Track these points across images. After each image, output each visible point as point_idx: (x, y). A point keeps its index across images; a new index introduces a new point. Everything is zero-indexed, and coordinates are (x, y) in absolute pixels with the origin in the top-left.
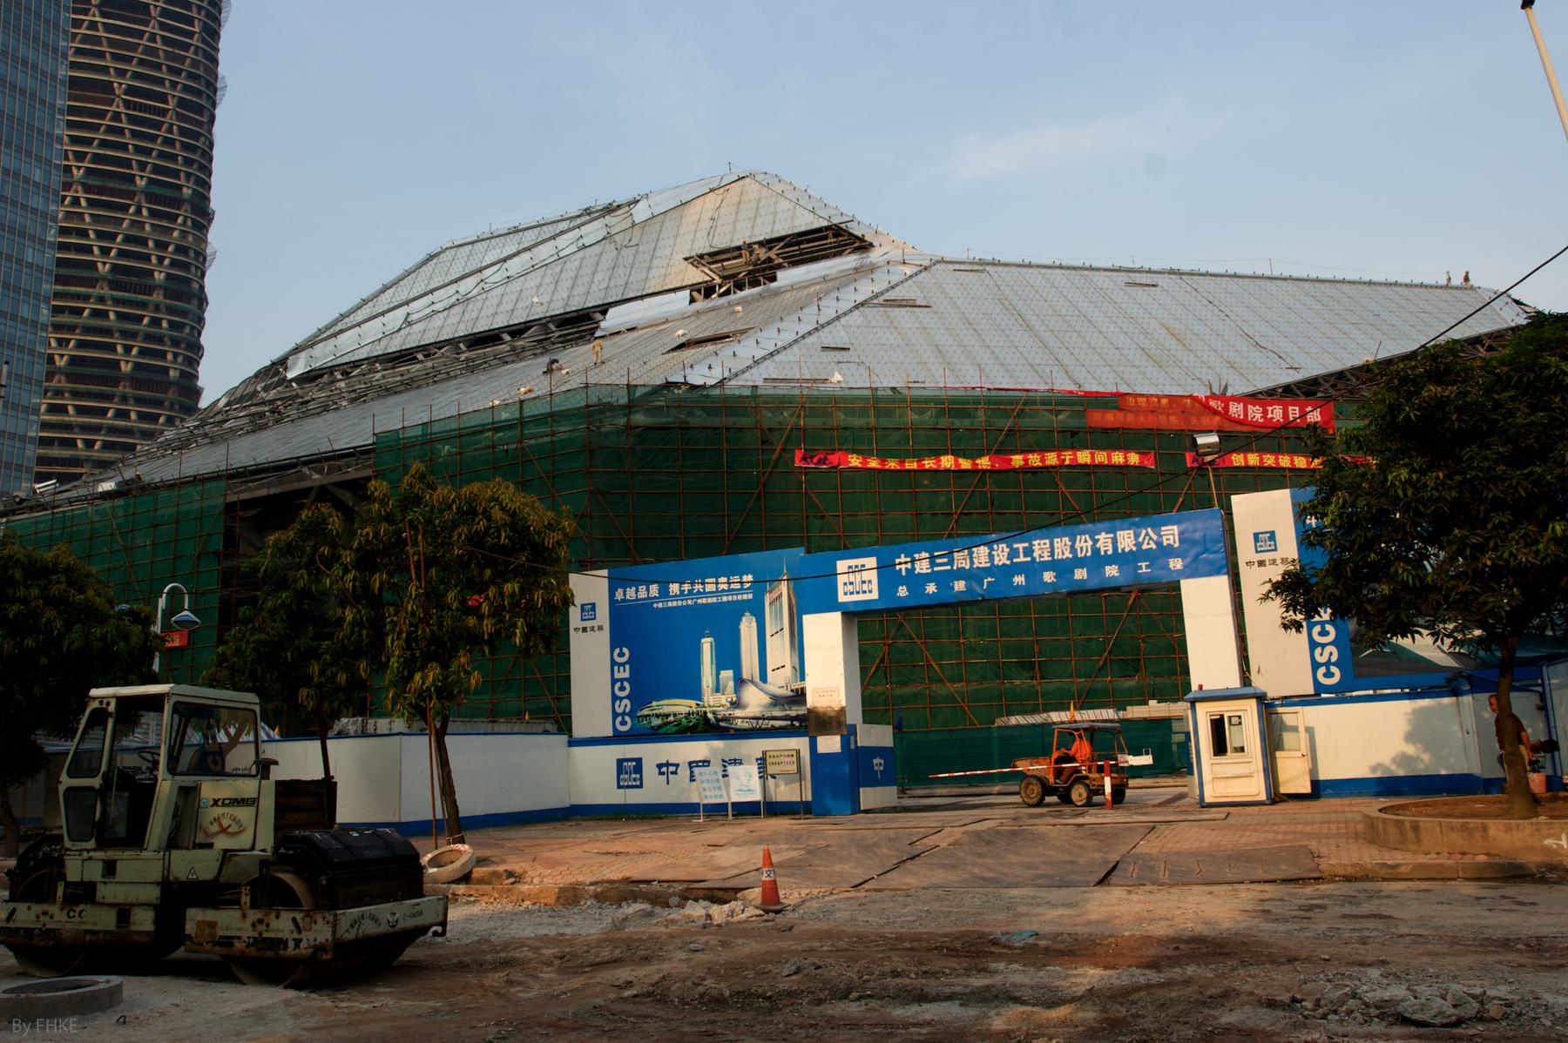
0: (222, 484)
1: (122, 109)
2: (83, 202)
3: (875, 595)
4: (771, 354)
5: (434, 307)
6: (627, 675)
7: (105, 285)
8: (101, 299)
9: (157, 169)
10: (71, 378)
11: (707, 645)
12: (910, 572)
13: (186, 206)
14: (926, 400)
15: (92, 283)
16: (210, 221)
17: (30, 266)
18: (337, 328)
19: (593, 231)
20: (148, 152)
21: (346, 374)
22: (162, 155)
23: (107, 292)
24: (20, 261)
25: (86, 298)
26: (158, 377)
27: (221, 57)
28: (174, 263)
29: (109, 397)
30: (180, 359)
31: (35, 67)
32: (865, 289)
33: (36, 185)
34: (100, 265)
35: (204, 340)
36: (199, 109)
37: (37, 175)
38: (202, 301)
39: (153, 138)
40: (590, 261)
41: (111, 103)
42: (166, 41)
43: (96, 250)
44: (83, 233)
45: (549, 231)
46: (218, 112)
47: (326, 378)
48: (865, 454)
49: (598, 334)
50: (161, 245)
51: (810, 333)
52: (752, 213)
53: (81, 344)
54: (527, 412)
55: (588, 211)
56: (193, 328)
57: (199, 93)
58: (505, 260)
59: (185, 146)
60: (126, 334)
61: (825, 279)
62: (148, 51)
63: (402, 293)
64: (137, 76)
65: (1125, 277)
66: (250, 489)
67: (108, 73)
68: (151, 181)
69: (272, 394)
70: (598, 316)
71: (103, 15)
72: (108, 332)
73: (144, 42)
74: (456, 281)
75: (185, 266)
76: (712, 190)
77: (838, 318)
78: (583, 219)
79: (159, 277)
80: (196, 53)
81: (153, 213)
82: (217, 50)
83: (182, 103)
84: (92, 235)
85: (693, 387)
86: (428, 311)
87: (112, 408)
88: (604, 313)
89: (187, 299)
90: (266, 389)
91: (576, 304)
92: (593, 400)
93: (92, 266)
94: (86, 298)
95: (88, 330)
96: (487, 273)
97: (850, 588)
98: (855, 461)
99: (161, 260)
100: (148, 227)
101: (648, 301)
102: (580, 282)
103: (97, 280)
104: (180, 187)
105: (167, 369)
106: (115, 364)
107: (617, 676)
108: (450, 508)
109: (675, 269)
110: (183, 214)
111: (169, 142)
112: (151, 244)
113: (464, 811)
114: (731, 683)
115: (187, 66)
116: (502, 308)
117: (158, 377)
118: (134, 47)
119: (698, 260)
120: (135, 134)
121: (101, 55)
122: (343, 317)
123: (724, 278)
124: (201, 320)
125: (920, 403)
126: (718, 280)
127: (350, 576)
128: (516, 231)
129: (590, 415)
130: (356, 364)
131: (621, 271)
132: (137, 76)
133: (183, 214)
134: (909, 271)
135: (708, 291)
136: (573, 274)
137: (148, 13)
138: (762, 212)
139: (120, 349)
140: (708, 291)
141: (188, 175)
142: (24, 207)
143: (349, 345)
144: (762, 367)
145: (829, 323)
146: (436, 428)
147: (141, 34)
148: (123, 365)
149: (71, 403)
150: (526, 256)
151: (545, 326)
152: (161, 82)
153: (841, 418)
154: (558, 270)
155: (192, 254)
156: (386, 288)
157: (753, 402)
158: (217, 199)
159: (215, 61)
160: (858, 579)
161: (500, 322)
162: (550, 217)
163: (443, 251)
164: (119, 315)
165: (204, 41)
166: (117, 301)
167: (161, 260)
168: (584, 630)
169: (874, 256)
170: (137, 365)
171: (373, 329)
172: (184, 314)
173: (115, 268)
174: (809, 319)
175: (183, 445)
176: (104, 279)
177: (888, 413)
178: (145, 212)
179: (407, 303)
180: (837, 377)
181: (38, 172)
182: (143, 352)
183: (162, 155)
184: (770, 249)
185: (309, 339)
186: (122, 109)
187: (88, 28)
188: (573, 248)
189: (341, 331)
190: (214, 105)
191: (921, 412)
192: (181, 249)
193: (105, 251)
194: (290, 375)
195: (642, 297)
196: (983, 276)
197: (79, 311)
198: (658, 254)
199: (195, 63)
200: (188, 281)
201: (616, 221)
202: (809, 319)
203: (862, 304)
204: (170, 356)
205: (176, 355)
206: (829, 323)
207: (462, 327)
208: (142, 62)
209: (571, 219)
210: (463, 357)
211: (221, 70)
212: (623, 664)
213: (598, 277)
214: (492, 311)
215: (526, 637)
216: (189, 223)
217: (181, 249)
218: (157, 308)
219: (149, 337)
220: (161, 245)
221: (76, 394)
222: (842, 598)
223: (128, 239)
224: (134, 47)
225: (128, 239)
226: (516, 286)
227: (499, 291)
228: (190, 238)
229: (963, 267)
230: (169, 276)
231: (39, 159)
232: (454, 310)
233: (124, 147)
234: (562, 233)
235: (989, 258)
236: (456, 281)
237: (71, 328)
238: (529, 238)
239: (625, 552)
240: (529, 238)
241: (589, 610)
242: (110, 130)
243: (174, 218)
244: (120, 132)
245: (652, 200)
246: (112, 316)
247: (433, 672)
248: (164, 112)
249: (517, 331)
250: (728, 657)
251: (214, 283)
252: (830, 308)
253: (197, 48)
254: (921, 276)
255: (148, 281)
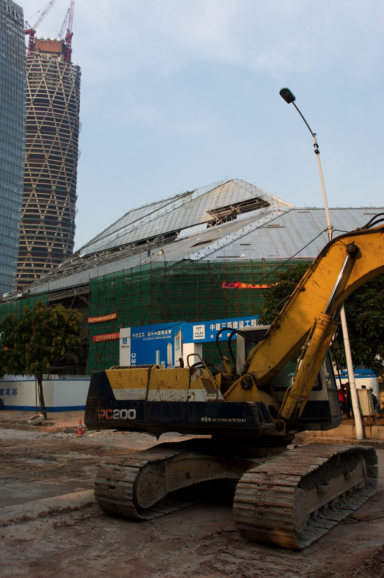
0: (46, 295)
1: (48, 164)
2: (36, 195)
3: (204, 338)
4: (222, 248)
5: (126, 232)
6: (135, 362)
7: (43, 223)
8: (42, 228)
9: (59, 183)
10: (33, 254)
11: (158, 352)
12: (215, 329)
13: (68, 195)
14: (273, 263)
15: (39, 222)
16: (76, 199)
17: (13, 220)
18: (97, 239)
19: (179, 203)
20: (56, 177)
21: (98, 255)
22: (60, 178)
23: (43, 225)
24: (11, 218)
25: (37, 227)
26: (60, 253)
27: (79, 143)
28: (65, 214)
29: (44, 260)
30: (67, 247)
31: (15, 155)
32: (262, 221)
33: (15, 193)
34: (41, 216)
35: (74, 240)
36: (72, 162)
37: (16, 190)
38: (74, 227)
39: (57, 173)
40: (176, 214)
41: (44, 162)
42: (61, 140)
43: (40, 211)
44: (36, 206)
45: (164, 203)
46: (78, 162)
47: (91, 257)
48: (248, 283)
49: (176, 240)
50: (61, 209)
51: (237, 239)
52: (231, 194)
53: (36, 243)
54: (133, 271)
55: (177, 196)
56: (71, 236)
57: (72, 156)
58: (149, 214)
59: (68, 175)
60: (49, 239)
61: (252, 218)
62: (56, 143)
63: (117, 227)
64: (52, 152)
65: (364, 211)
66: (57, 297)
67: (43, 152)
68: (57, 187)
69: (75, 263)
70: (177, 233)
71: (41, 133)
72: (44, 238)
73: (54, 141)
74: (133, 222)
75: (68, 215)
76: (218, 186)
77: (249, 233)
78: (176, 199)
79: (60, 219)
80: (71, 143)
81: (57, 198)
82: (77, 141)
83: (67, 160)
84: (39, 206)
85: (192, 261)
86: (124, 233)
87: (45, 264)
88: (179, 232)
89: (69, 226)
90: (73, 261)
91: (170, 229)
92: (154, 267)
93: (39, 216)
94: (37, 227)
95: (38, 238)
96: (144, 219)
97: (197, 335)
98: (244, 286)
99: (60, 213)
100: (56, 203)
101: (194, 227)
102: (172, 221)
103: (40, 221)
104: (66, 188)
105: (62, 250)
106: (46, 249)
107: (132, 362)
108: (42, 315)
109: (204, 216)
110: (67, 197)
111: (63, 173)
112: (57, 208)
113: (46, 405)
114: (164, 366)
115: (68, 147)
116: (147, 231)
117: (60, 253)
118: (51, 143)
119: (211, 212)
120: (52, 172)
121: (41, 146)
122: (98, 236)
123: (219, 218)
124: (73, 233)
125: (271, 264)
126: (217, 219)
127: (16, 335)
128: (154, 204)
129: (152, 272)
130: (101, 252)
131: (186, 217)
132: (52, 152)
133: (67, 197)
134: (280, 214)
135: (214, 223)
136: (171, 219)
137: (55, 131)
138: (234, 194)
139: (48, 244)
140: (214, 223)
141: (69, 184)
142: (12, 201)
143: (100, 246)
144: (217, 253)
145: (245, 235)
146: (107, 277)
147: (53, 138)
148: (49, 249)
149: (32, 263)
150: (156, 213)
151: (160, 237)
152: (59, 153)
153: (242, 271)
154: (166, 217)
155: (70, 211)
156: (112, 225)
157: (208, 266)
158: (78, 192)
159: (77, 145)
160: (199, 331)
161: (146, 236)
162: (165, 198)
163: (131, 212)
164: (47, 233)
165: (73, 138)
166: (47, 228)
167: (60, 213)
168: (124, 347)
169: (270, 208)
170: (53, 249)
171: (106, 240)
172: (68, 231)
173: (46, 217)
174: (240, 233)
175: (47, 280)
176: (42, 221)
177: (259, 267)
178: (55, 198)
179: (118, 231)
180: (243, 255)
181: (16, 189)
182: (55, 245)
183: (60, 178)
184: (236, 207)
185: (87, 244)
186: (48, 164)
187: (37, 138)
188: (172, 209)
189: (97, 241)
190: (77, 160)
191: (271, 267)
192: (67, 209)
193: (43, 211)
194: (81, 256)
195: (192, 226)
196: (308, 214)
197: (35, 232)
198: (198, 210)
199: (71, 146)
200: (69, 220)
201: (187, 199)
202: (240, 233)
203: (259, 227)
204: (63, 246)
205: (65, 245)
206: (245, 235)
207: (134, 238)
208: (54, 147)
209: (172, 199)
210: (133, 249)
211: (79, 148)
212: (134, 358)
213: (179, 219)
214: (144, 232)
215: (65, 352)
216: (69, 200)
217: (67, 209)
218: (59, 230)
219: (57, 240)
220: (61, 209)
221: (34, 260)
222: (194, 338)
223: (50, 207)
224: (51, 143)
225: (50, 207)
226: (152, 223)
227: (146, 226)
228: (70, 205)
229: (301, 211)
230: (63, 219)
231: (16, 184)
232: (132, 233)
233: (48, 176)
234: (169, 204)
235: (312, 207)
236: (133, 222)
237: (32, 238)
238: (158, 206)
239: (139, 320)
240: (158, 206)
241: (125, 340)
242: (44, 171)
243: (64, 199)
244: (47, 171)
245: (198, 191)
246: (45, 233)
247: (37, 363)
248: (61, 164)
249: (151, 239)
250: (163, 357)
251: (78, 220)
252: (247, 229)
253: (71, 141)
254: (284, 216)
255: (56, 221)
